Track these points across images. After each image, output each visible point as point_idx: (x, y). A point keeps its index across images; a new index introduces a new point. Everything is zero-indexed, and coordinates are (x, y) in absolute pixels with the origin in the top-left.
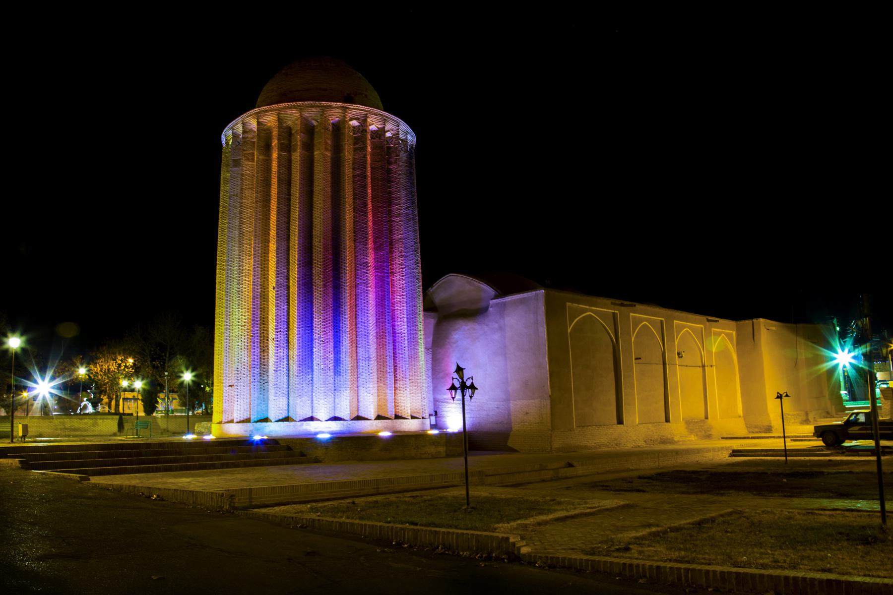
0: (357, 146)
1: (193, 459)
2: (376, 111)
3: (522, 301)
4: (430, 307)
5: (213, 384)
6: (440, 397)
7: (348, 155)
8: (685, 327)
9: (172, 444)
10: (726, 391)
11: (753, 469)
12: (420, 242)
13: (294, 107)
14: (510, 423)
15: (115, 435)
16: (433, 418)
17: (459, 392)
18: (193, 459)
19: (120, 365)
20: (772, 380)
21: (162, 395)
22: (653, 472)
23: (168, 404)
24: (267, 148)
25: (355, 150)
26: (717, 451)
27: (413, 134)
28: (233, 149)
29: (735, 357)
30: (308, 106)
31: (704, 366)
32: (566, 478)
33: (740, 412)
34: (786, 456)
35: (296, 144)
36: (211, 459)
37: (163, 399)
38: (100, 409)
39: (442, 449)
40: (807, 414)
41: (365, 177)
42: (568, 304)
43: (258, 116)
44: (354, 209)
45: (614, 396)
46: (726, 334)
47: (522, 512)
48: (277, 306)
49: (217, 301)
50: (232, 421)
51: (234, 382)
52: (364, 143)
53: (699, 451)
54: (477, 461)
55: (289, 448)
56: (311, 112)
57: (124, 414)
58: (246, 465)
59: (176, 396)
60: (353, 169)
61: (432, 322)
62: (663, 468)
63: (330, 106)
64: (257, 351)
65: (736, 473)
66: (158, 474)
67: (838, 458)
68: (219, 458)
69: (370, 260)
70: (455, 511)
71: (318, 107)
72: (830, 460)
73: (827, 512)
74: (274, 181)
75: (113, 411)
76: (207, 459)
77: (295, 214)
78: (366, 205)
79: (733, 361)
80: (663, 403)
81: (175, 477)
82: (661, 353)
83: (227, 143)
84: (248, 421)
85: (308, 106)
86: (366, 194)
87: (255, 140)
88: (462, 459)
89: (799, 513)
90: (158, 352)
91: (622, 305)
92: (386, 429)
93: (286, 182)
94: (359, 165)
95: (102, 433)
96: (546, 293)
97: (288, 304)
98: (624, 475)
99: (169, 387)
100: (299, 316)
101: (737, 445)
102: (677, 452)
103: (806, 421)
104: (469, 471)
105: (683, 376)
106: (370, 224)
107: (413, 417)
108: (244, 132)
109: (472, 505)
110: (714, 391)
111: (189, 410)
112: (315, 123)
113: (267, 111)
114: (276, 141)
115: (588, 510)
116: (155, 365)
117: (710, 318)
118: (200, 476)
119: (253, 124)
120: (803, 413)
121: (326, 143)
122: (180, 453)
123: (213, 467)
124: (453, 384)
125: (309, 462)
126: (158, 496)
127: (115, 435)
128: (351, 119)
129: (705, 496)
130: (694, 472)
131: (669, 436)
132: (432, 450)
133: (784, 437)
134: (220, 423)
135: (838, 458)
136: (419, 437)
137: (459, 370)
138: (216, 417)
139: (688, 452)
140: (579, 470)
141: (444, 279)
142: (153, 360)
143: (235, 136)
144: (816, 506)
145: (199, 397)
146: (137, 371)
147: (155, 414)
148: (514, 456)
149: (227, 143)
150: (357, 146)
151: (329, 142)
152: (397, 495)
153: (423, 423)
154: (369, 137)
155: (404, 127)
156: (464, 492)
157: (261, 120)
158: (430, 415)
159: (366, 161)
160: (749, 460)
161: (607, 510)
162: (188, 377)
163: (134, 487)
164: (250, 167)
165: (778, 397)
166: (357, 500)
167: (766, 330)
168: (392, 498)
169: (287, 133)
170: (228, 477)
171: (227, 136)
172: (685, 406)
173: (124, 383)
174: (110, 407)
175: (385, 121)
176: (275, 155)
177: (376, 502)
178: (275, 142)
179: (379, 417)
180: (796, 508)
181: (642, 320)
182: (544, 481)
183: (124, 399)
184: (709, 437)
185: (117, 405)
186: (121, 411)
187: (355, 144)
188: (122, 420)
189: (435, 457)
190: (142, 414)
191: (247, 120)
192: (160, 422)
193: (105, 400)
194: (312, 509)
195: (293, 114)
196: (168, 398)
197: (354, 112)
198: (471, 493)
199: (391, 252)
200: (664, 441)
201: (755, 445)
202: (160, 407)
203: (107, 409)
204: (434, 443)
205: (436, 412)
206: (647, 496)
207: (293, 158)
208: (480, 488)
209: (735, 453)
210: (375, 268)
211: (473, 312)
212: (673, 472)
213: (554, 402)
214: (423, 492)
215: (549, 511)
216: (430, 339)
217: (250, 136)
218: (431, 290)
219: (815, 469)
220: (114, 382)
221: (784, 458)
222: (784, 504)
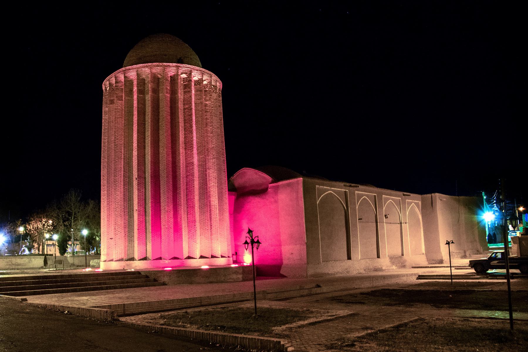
0: (186, 90)
1: (89, 284)
2: (197, 68)
3: (288, 185)
4: (232, 189)
5: (100, 235)
6: (239, 244)
7: (181, 96)
8: (389, 199)
9: (76, 275)
10: (414, 241)
11: (431, 288)
12: (226, 149)
13: (147, 67)
14: (281, 260)
15: (42, 268)
16: (235, 257)
17: (250, 245)
18: (89, 284)
19: (44, 225)
20: (444, 234)
21: (70, 243)
22: (370, 290)
23: (74, 247)
25: (185, 92)
26: (409, 276)
28: (110, 93)
29: (420, 217)
30: (155, 66)
31: (401, 223)
32: (316, 294)
33: (424, 251)
34: (452, 279)
35: (148, 90)
36: (100, 284)
37: (71, 245)
38: (33, 251)
39: (240, 276)
40: (465, 252)
41: (191, 109)
42: (317, 186)
43: (124, 72)
44: (185, 129)
45: (345, 228)
46: (415, 203)
47: (289, 319)
48: (138, 190)
50: (112, 260)
51: (113, 236)
52: (190, 88)
53: (398, 276)
54: (262, 284)
55: (147, 277)
56: (157, 68)
57: (47, 255)
58: (121, 287)
59: (78, 243)
60: (184, 104)
61: (234, 197)
62: (376, 287)
63: (169, 66)
64: (127, 217)
65: (420, 291)
66: (69, 294)
67: (484, 281)
70: (248, 318)
71: (161, 66)
72: (479, 282)
73: (477, 320)
74: (135, 113)
75: (41, 253)
76: (98, 284)
78: (192, 127)
79: (419, 219)
80: (376, 246)
81: (79, 296)
82: (374, 216)
83: (106, 89)
84: (121, 260)
85: (155, 66)
87: (123, 87)
88: (252, 282)
89: (459, 320)
90: (67, 216)
91: (350, 186)
92: (206, 264)
93: (142, 113)
95: (34, 267)
96: (304, 182)
97: (145, 189)
98: (351, 292)
99: (74, 237)
100: (151, 196)
101: (421, 271)
102: (384, 277)
103: (465, 257)
104: (256, 291)
105: (388, 230)
107: (222, 257)
108: (116, 82)
109: (258, 314)
110: (407, 238)
111: (86, 252)
112: (160, 76)
113: (130, 69)
114: (136, 88)
115: (329, 318)
116: (65, 224)
117: (405, 193)
118: (93, 295)
119: (122, 77)
120: (462, 251)
121: (167, 88)
122: (82, 281)
123: (102, 289)
125: (159, 285)
126: (68, 312)
127: (42, 268)
128: (182, 74)
129: (401, 308)
130: (394, 290)
131: (380, 267)
132: (234, 276)
133: (451, 267)
134: (105, 261)
135: (484, 281)
136: (226, 269)
137: (250, 231)
138: (103, 258)
139: (391, 277)
140: (324, 289)
142: (64, 221)
143: (110, 85)
144: (470, 315)
145: (91, 244)
146: (55, 229)
147: (66, 255)
148: (284, 280)
149: (106, 89)
150: (186, 90)
151: (169, 88)
152: (213, 307)
153: (229, 260)
154: (193, 84)
155: (215, 77)
156: (253, 305)
157: (126, 75)
158: (233, 255)
159: (191, 99)
160: (429, 282)
161: (341, 317)
162: (85, 232)
163: (54, 306)
164: (120, 104)
165: (447, 244)
166: (189, 311)
167: (440, 200)
168: (210, 309)
169: (142, 82)
170: (111, 296)
171: (106, 85)
172: (389, 248)
173: (47, 236)
174: (39, 250)
175: (203, 74)
176: (135, 97)
177: (200, 311)
178: (135, 89)
179: (202, 257)
180: (458, 317)
181: (363, 195)
182: (302, 296)
183: (47, 245)
184: (404, 266)
185: (43, 249)
186: (46, 253)
188: (46, 258)
189: (235, 281)
190: (58, 254)
192: (69, 259)
193: (36, 245)
194: (161, 317)
196: (74, 245)
198: (258, 305)
200: (376, 270)
201: (433, 272)
202: (69, 250)
203: (37, 252)
204: (235, 273)
206: (365, 307)
207: (146, 98)
208: (264, 301)
209: (420, 277)
211: (260, 191)
212: (382, 290)
213: (308, 247)
214: (228, 304)
215: (305, 318)
217: (120, 85)
219: (470, 288)
220: (41, 234)
221: (450, 281)
222: (450, 314)
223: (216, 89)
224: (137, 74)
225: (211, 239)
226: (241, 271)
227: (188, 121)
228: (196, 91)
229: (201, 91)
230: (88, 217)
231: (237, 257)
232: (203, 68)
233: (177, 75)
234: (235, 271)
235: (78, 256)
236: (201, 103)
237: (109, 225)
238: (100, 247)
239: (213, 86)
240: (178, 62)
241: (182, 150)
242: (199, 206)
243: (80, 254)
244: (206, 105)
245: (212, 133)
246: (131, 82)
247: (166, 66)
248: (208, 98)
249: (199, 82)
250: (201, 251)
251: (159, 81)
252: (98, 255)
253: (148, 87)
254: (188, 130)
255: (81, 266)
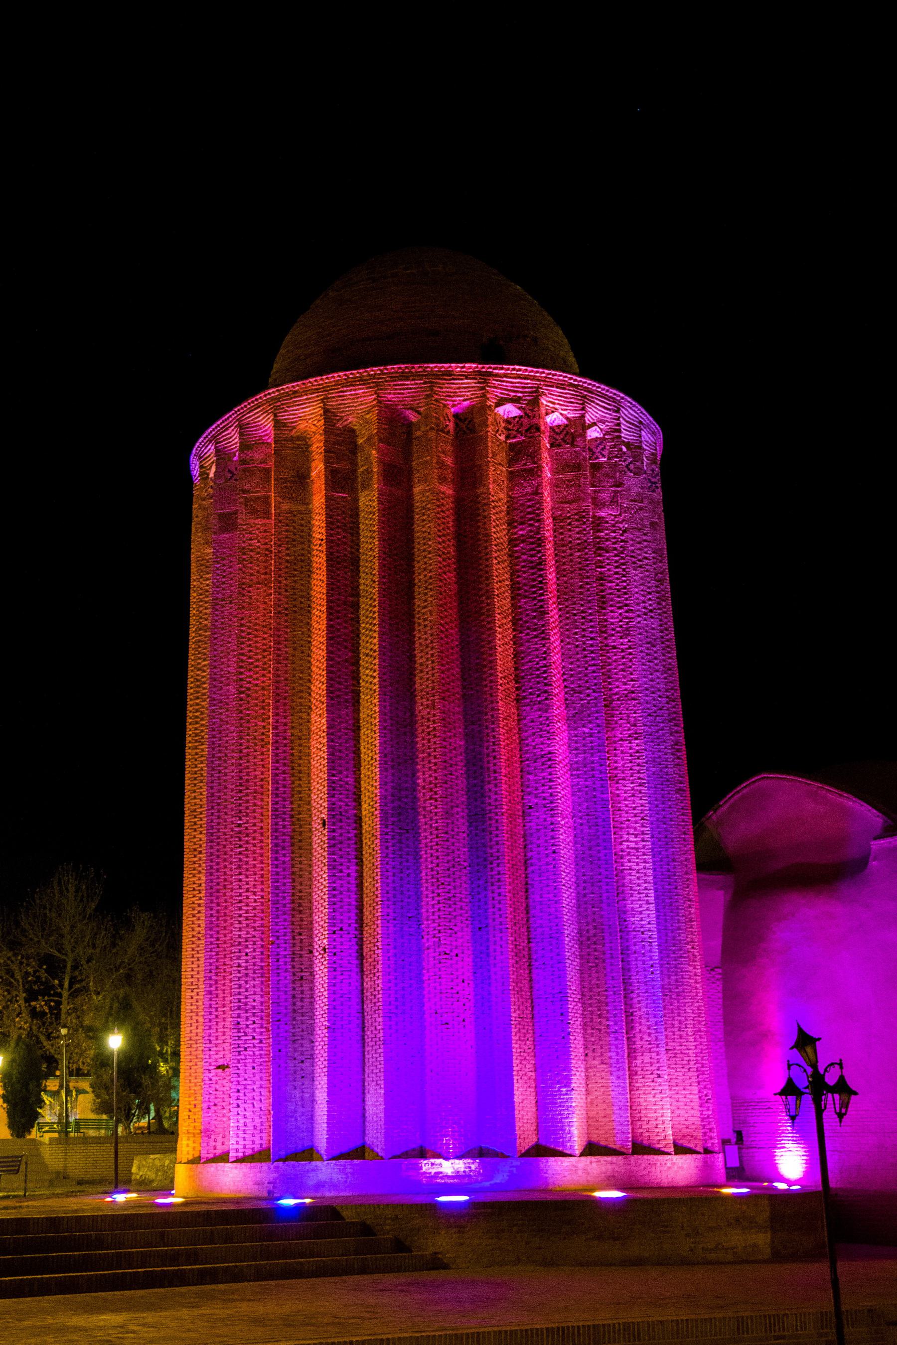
0: (515, 468)
2: (566, 377)
4: (712, 862)
5: (176, 1054)
7: (497, 489)
13: (363, 381)
16: (733, 1149)
24: (300, 481)
25: (512, 476)
27: (656, 427)
36: (174, 1258)
41: (540, 542)
44: (515, 622)
49: (188, 857)
50: (223, 1157)
52: (535, 456)
55: (365, 1229)
56: (403, 386)
59: (85, 1084)
61: (720, 898)
68: (192, 1257)
69: (560, 746)
71: (419, 376)
74: (319, 560)
77: (370, 642)
78: (542, 613)
86: (542, 584)
87: (271, 464)
92: (611, 1182)
94: (524, 512)
106: (556, 658)
107: (680, 1149)
108: (245, 446)
111: (118, 1122)
112: (413, 418)
114: (321, 466)
119: (265, 422)
121: (441, 465)
122: (100, 1244)
124: (790, 1082)
132: (737, 1239)
136: (696, 1198)
137: (804, 1040)
138: (186, 1146)
141: (744, 788)
145: (137, 1088)
149: (204, 475)
150: (515, 468)
151: (449, 460)
155: (632, 411)
158: (725, 1142)
159: (540, 502)
171: (204, 461)
175: (583, 400)
176: (318, 501)
178: (318, 469)
179: (592, 1149)
187: (511, 462)
191: (250, 417)
195: (359, 401)
197: (507, 383)
199: (610, 725)
205: (739, 1134)
210: (572, 767)
216: (717, 943)
218: (713, 816)
223: (637, 458)
224: (326, 411)
225: (632, 1054)
226: (764, 1216)
227: (526, 589)
228: (560, 466)
229: (577, 467)
230: (128, 978)
231: (746, 1157)
232: (581, 374)
233: (482, 409)
234: (738, 1214)
235: (86, 1140)
236: (581, 516)
237: (212, 1015)
238: (172, 1102)
239: (628, 445)
240: (485, 360)
241: (505, 709)
242: (580, 932)
243: (92, 1133)
244: (598, 524)
245: (626, 632)
246: (302, 444)
247: (437, 376)
248: (605, 496)
249: (571, 433)
250: (590, 1121)
251: (409, 433)
252: (164, 1136)
253: (368, 458)
254: (529, 624)
255: (91, 1182)
